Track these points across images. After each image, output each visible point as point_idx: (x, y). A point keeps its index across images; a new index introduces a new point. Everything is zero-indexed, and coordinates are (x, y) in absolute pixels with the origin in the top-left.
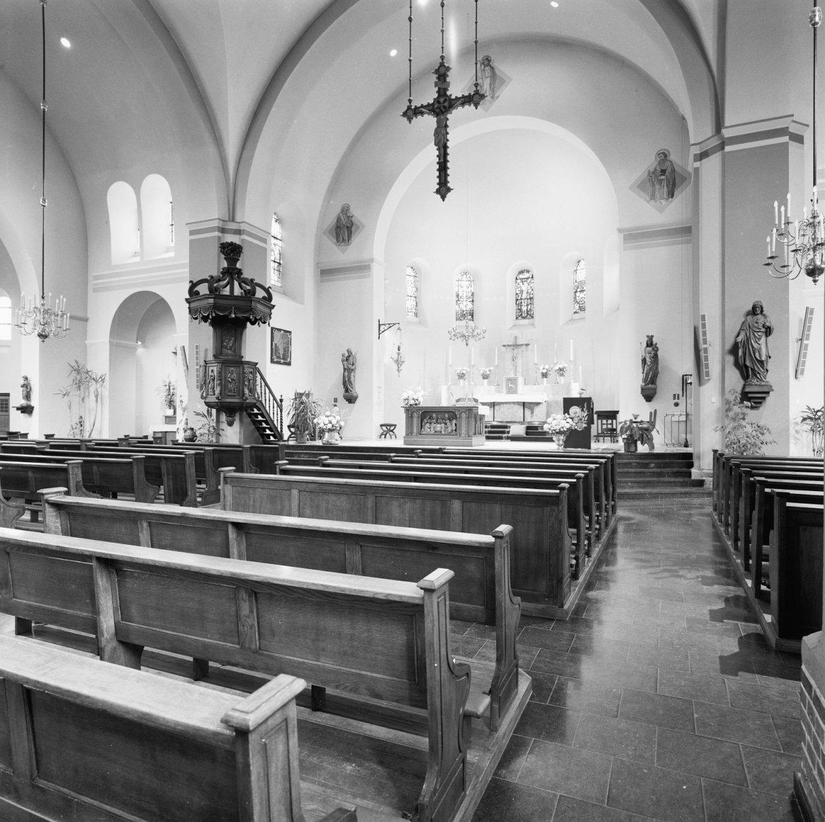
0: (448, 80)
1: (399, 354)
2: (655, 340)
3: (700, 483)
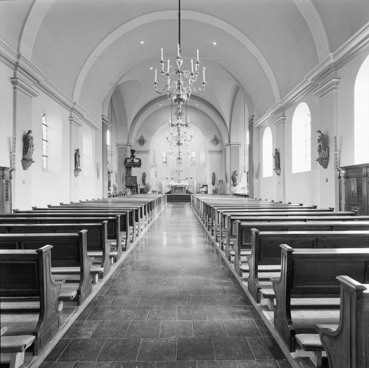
2: (214, 173)
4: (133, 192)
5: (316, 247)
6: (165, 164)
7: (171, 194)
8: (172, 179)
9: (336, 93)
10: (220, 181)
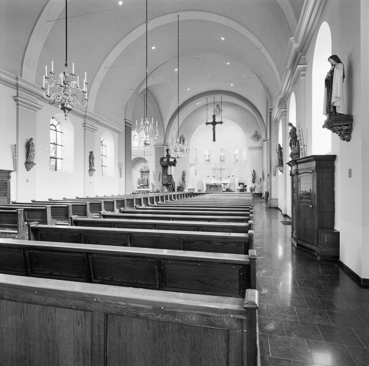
2: (255, 171)
3: (264, 198)
6: (207, 162)
9: (304, 80)
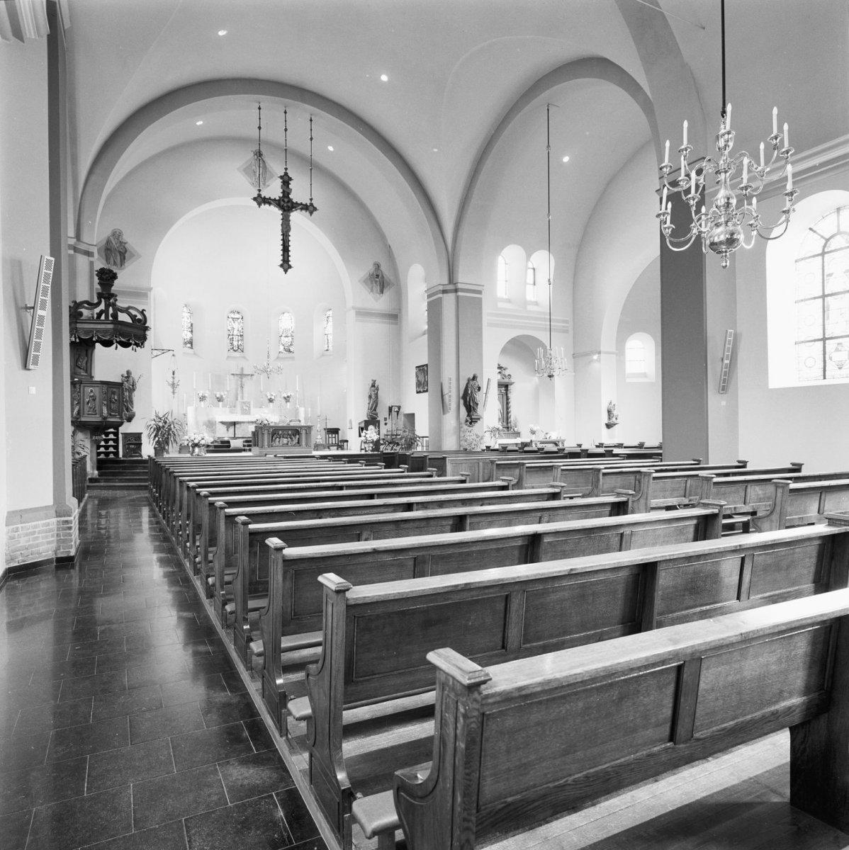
0: (290, 186)
1: (173, 378)
4: (99, 447)
5: (411, 576)
7: (343, 449)
8: (220, 399)
10: (390, 409)
